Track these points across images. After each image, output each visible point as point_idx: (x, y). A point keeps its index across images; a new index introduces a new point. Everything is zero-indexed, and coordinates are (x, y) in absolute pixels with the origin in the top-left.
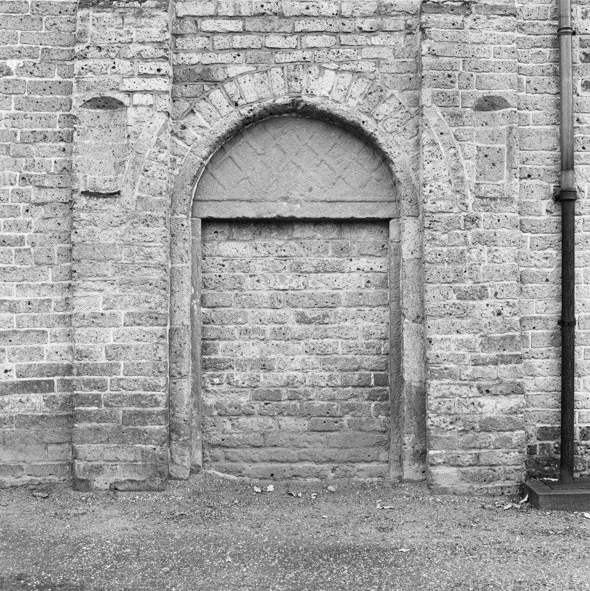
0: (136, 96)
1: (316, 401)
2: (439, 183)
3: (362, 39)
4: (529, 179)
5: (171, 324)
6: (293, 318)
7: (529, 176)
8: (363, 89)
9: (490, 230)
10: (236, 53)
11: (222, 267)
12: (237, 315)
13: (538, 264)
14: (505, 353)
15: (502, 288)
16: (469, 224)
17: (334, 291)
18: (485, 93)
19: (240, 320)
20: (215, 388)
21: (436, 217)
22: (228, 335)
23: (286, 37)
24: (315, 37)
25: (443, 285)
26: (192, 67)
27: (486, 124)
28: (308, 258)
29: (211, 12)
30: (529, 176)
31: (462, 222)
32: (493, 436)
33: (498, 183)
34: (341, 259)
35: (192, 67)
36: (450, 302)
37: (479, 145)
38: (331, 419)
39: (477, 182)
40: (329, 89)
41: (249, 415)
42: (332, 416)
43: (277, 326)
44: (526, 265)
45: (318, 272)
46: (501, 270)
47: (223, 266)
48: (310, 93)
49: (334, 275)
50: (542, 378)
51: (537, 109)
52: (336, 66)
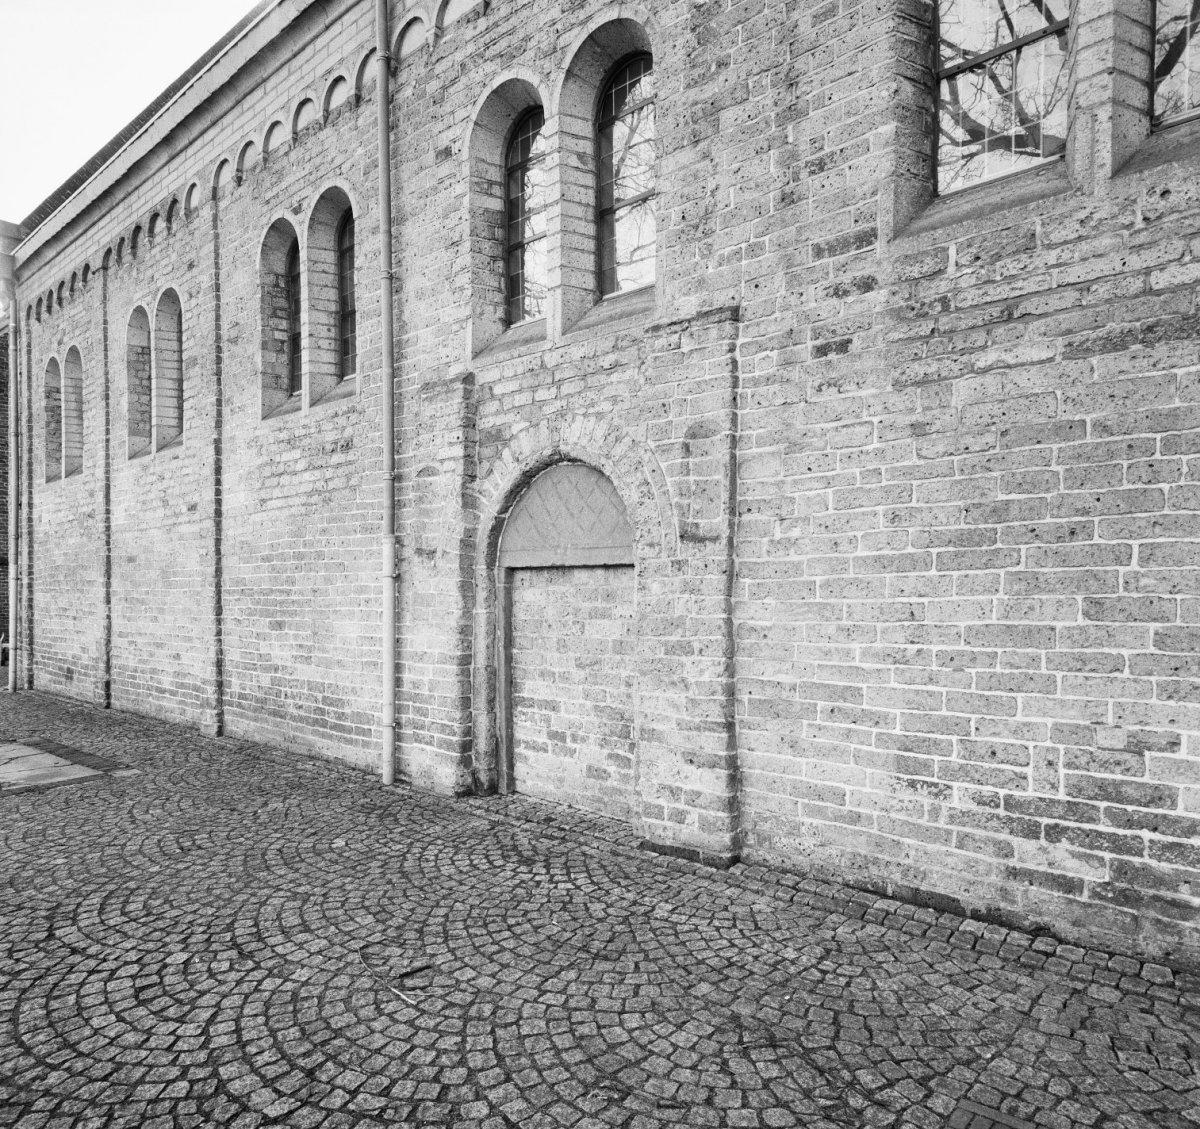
3: (603, 378)
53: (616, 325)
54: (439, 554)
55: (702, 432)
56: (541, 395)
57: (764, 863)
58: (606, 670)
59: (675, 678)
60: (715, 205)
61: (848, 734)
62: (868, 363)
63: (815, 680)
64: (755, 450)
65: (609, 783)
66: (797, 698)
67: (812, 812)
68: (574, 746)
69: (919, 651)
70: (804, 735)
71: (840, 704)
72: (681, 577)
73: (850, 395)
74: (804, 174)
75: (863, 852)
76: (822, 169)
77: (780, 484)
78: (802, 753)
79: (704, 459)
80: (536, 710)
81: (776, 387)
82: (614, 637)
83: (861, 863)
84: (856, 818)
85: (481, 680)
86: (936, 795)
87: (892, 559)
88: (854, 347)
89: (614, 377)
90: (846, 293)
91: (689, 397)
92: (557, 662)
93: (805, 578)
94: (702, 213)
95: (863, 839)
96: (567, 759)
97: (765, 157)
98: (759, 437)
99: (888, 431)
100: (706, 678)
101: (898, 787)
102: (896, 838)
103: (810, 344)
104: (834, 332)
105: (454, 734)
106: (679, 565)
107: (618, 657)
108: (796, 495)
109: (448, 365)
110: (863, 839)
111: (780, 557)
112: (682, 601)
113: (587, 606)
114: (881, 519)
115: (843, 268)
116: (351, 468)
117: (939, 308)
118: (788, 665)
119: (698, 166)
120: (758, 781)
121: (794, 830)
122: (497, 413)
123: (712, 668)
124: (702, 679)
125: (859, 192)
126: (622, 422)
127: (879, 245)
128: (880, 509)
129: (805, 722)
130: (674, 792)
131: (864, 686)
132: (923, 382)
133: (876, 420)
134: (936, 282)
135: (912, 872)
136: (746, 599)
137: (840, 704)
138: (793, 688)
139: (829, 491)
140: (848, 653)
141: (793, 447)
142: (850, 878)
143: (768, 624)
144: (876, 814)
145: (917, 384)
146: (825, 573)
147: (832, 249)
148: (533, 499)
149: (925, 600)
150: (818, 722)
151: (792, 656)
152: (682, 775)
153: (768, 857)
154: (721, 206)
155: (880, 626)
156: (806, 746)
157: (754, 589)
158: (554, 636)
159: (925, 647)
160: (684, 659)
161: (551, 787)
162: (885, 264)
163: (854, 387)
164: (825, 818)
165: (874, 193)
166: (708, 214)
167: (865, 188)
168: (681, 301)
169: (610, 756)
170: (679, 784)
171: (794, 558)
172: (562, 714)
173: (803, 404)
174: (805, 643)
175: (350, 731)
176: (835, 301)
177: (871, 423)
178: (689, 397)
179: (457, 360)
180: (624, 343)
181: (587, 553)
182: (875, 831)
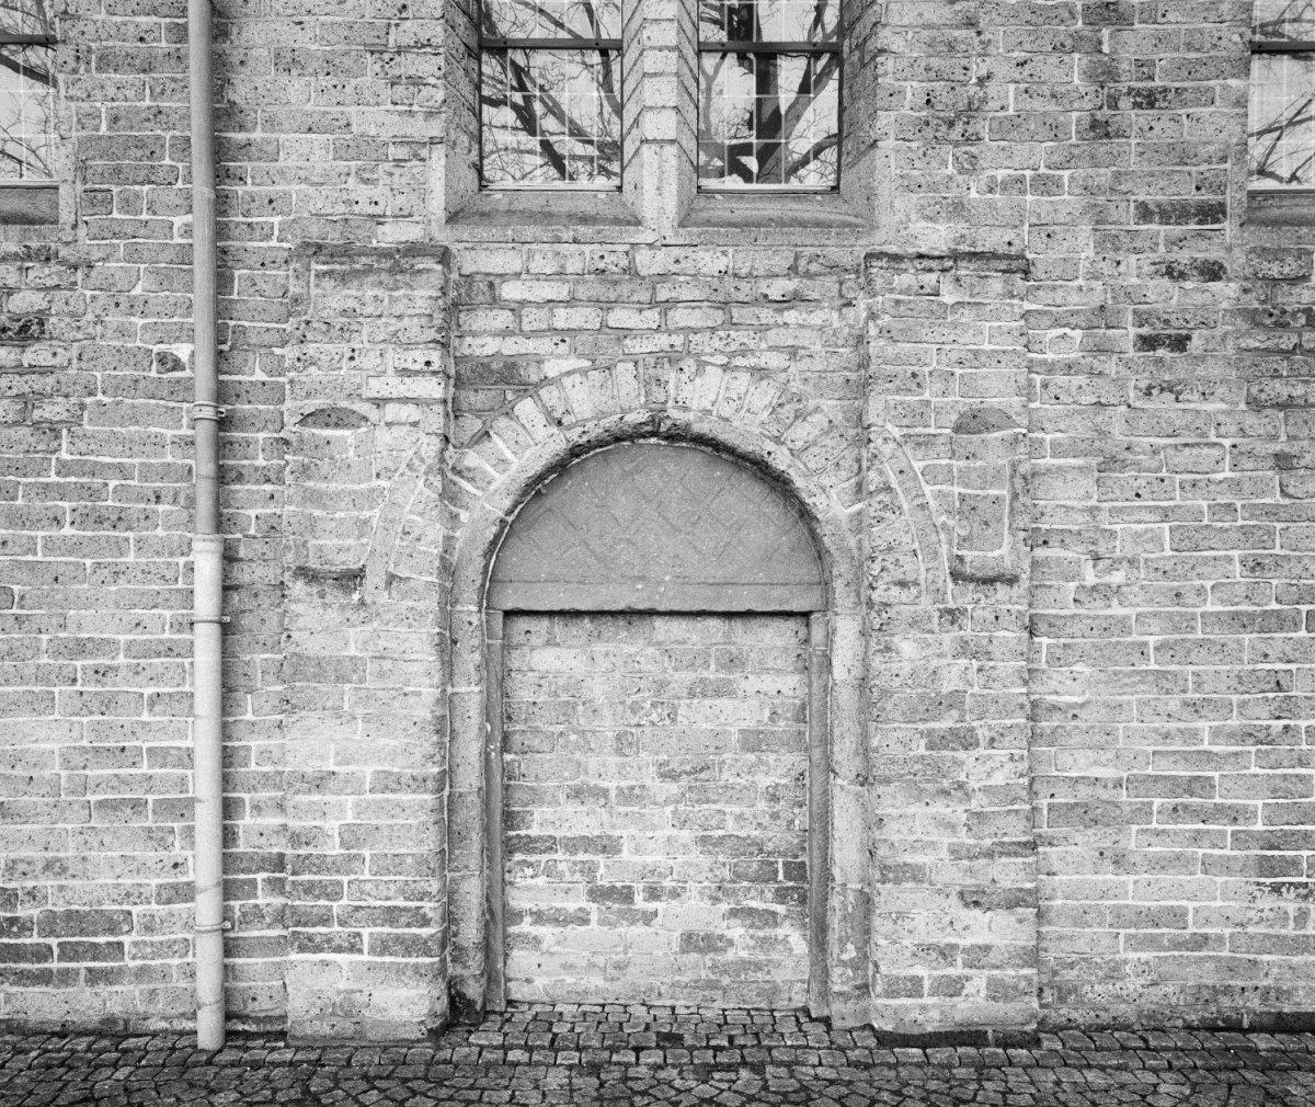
3: (767, 315)
40: (713, 398)
53: (798, 236)
54: (374, 579)
55: (973, 424)
56: (620, 317)
57: (1070, 1024)
58: (727, 776)
59: (946, 783)
60: (984, 100)
61: (1197, 837)
62: (1214, 370)
63: (1150, 771)
64: (1050, 461)
65: (730, 955)
66: (1123, 796)
67: (1137, 943)
68: (652, 906)
69: (1286, 727)
70: (1132, 846)
71: (1186, 800)
72: (957, 633)
73: (1192, 406)
74: (1125, 103)
75: (1210, 982)
76: (1151, 105)
77: (1092, 511)
78: (1131, 868)
79: (971, 463)
80: (559, 856)
81: (1081, 379)
82: (744, 725)
83: (1202, 995)
84: (1202, 941)
85: (470, 814)
86: (1306, 897)
87: (1252, 616)
88: (1196, 345)
89: (791, 316)
90: (1182, 276)
91: (958, 371)
92: (605, 770)
93: (1135, 637)
94: (961, 106)
95: (1210, 966)
96: (638, 930)
97: (1066, 58)
98: (1054, 444)
99: (1244, 459)
100: (998, 779)
101: (1258, 894)
102: (1251, 957)
103: (1133, 331)
104: (1167, 322)
105: (425, 922)
106: (953, 616)
107: (751, 757)
108: (1117, 527)
109: (378, 220)
110: (1210, 966)
111: (1097, 608)
112: (954, 669)
113: (687, 676)
114: (1238, 567)
115: (1179, 242)
116: (38, 383)
117: (1303, 321)
118: (1110, 755)
119: (956, 33)
120: (1059, 915)
121: (1114, 972)
122: (505, 333)
123: (1011, 765)
124: (992, 782)
125: (1204, 152)
126: (809, 388)
127: (1229, 227)
128: (1236, 553)
129: (1135, 828)
130: (946, 953)
131: (1216, 775)
132: (1286, 405)
133: (1227, 443)
134: (1296, 290)
135: (1273, 994)
136: (1044, 666)
137: (1186, 800)
138: (1118, 784)
139: (1166, 526)
140: (1194, 735)
141: (1110, 463)
142: (1193, 1018)
143: (1080, 700)
144: (1227, 932)
145: (1279, 406)
146: (1163, 632)
147: (1166, 214)
148: (577, 494)
149: (1293, 667)
150: (1154, 825)
151: (1116, 740)
152: (958, 926)
153: (1074, 1015)
154: (992, 105)
155: (1235, 698)
156: (1138, 859)
157: (1058, 653)
158: (608, 726)
159: (1292, 723)
160: (961, 755)
161: (596, 981)
162: (1237, 252)
163: (1196, 396)
164: (1161, 948)
165: (1224, 159)
166: (971, 109)
167: (1211, 149)
168: (918, 226)
169: (733, 913)
170: (953, 940)
171: (1117, 610)
172: (625, 855)
173: (1123, 408)
174: (1135, 724)
175: (42, 953)
176: (1166, 282)
177: (1221, 445)
178: (958, 371)
179: (403, 215)
180: (814, 267)
181: (709, 592)
182: (1226, 953)
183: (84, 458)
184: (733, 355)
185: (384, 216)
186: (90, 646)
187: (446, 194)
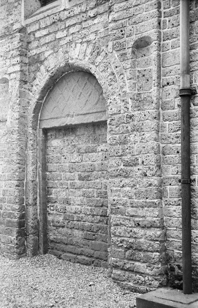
0: (12, 75)
1: (86, 223)
2: (114, 97)
3: (90, 22)
4: (168, 86)
5: (26, 180)
6: (77, 177)
7: (168, 84)
8: (91, 50)
9: (140, 122)
10: (47, 45)
11: (53, 152)
12: (57, 176)
13: (173, 141)
14: (148, 200)
15: (146, 158)
16: (128, 119)
17: (93, 162)
18: (139, 36)
19: (59, 178)
20: (52, 212)
21: (113, 117)
22: (55, 186)
23: (63, 31)
24: (73, 28)
25: (117, 157)
26: (34, 57)
27: (145, 55)
28: (82, 145)
29: (38, 28)
30: (168, 84)
31: (125, 119)
32: (142, 254)
33: (150, 91)
34: (95, 145)
35: (34, 57)
36: (120, 168)
37: (139, 69)
38: (92, 233)
39: (139, 93)
40: (78, 54)
41: (63, 227)
42: (92, 232)
43: (72, 181)
44: (165, 142)
45: (86, 153)
46: (146, 147)
47: (54, 151)
48: (71, 58)
49: (92, 154)
50: (176, 218)
51: (174, 38)
52: (80, 40)
109: (12, 24)
179: (17, 21)
183: (38, 125)
184: (82, 39)
185: (14, 23)
186: (134, 291)
187: (24, 13)
